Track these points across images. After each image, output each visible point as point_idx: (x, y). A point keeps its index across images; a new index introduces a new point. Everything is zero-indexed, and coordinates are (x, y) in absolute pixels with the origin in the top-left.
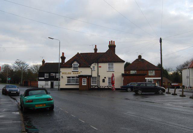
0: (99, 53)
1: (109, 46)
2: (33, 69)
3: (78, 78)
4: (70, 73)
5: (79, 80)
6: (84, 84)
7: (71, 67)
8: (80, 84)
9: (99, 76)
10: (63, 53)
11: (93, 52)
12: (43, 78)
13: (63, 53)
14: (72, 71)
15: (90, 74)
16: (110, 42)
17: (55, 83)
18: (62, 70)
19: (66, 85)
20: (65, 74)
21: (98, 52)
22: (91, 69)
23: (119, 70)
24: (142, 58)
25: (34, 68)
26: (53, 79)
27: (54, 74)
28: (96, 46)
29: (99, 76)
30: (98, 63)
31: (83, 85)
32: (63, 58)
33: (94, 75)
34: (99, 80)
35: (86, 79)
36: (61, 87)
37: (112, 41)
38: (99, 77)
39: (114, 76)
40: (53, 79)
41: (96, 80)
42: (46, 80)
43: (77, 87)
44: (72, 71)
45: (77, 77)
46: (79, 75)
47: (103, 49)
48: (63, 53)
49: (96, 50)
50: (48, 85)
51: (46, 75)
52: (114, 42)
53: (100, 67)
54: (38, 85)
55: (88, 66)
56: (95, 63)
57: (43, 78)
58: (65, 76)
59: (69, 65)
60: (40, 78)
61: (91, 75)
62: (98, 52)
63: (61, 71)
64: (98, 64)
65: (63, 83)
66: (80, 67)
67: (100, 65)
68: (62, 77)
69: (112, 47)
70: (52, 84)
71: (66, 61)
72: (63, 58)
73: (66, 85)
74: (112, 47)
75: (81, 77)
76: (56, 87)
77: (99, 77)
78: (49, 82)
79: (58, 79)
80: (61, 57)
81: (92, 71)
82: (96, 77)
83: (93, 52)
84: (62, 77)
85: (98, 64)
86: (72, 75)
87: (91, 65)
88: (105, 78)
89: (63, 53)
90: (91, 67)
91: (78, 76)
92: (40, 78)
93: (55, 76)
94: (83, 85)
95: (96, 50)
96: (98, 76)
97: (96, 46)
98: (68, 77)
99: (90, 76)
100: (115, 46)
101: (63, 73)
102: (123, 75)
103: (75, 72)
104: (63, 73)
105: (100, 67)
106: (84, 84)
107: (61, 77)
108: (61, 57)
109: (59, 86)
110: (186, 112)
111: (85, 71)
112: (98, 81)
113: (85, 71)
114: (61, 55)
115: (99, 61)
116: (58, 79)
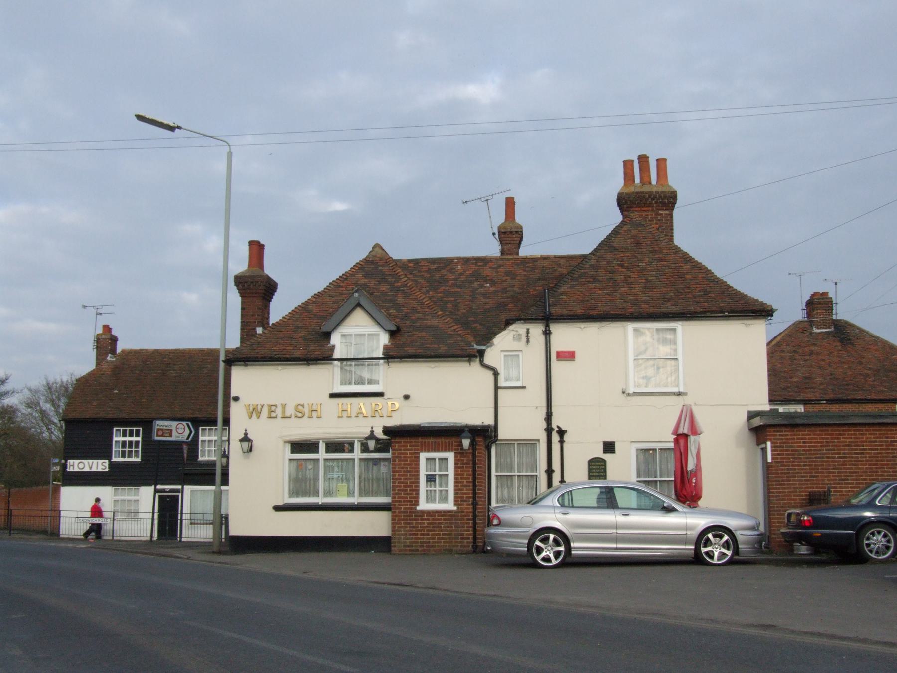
0: (534, 260)
1: (625, 202)
2: (43, 413)
3: (382, 446)
4: (315, 412)
5: (384, 469)
6: (437, 497)
7: (325, 357)
8: (401, 504)
9: (561, 433)
10: (252, 244)
11: (493, 249)
12: (100, 465)
13: (257, 249)
14: (333, 396)
15: (482, 417)
16: (628, 164)
17: (193, 499)
18: (249, 384)
19: (277, 509)
20: (272, 405)
21: (525, 251)
22: (489, 374)
23: (719, 374)
24: (842, 313)
25: (47, 407)
26: (173, 468)
27: (180, 431)
28: (510, 204)
29: (555, 433)
30: (547, 319)
31: (424, 505)
32: (256, 289)
33: (520, 422)
34: (556, 465)
35: (450, 456)
36: (236, 530)
37: (643, 160)
38: (555, 438)
39: (694, 430)
40: (173, 468)
41: (534, 467)
42: (120, 476)
43: (375, 525)
44: (333, 396)
45: (372, 444)
46: (392, 423)
47: (573, 220)
48: (257, 249)
49: (510, 236)
50: (133, 514)
51: (125, 445)
52: (661, 162)
53: (569, 356)
54: (56, 514)
55: (463, 341)
56: (519, 328)
57: (100, 465)
58: (272, 437)
59: (303, 341)
60: (76, 465)
61: (491, 422)
62: (525, 251)
63: (233, 394)
64: (547, 333)
65: (255, 498)
66: (390, 356)
67: (565, 335)
68: (246, 439)
69: (647, 204)
70: (168, 509)
71: (279, 308)
72: (256, 289)
73: (277, 509)
74: (647, 204)
75: (404, 438)
76: (194, 532)
77: (555, 438)
78: (145, 498)
79: (212, 475)
80: (241, 282)
81: (497, 388)
82: (532, 444)
83: (493, 249)
84: (246, 439)
85: (547, 333)
86: (331, 423)
87: (487, 338)
88: (609, 447)
89: (252, 244)
90: (493, 356)
91: (387, 431)
92: (76, 465)
93: (194, 444)
94: (424, 505)
95: (510, 236)
96: (549, 430)
97: (510, 204)
98: (298, 446)
99: (485, 435)
100: (668, 200)
101: (254, 412)
102: (760, 429)
103: (361, 401)
104: (254, 412)
105: (569, 356)
106: (437, 497)
107: (235, 448)
108: (241, 282)
109: (222, 521)
110: (485, 595)
111: (442, 393)
112: (550, 472)
113: (442, 393)
114: (240, 264)
115: (556, 310)
116: (212, 475)
